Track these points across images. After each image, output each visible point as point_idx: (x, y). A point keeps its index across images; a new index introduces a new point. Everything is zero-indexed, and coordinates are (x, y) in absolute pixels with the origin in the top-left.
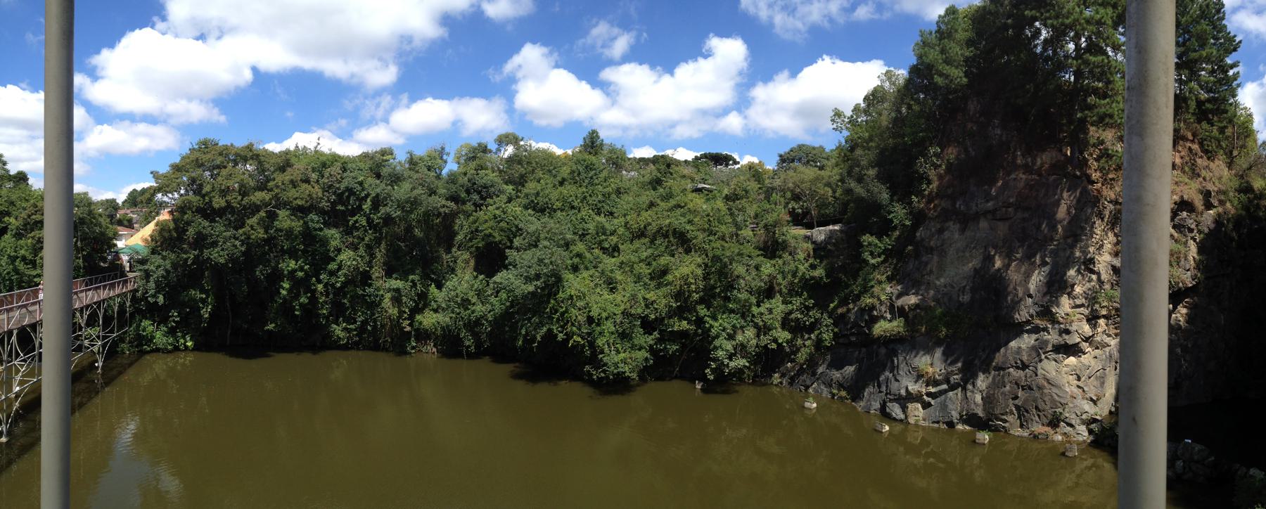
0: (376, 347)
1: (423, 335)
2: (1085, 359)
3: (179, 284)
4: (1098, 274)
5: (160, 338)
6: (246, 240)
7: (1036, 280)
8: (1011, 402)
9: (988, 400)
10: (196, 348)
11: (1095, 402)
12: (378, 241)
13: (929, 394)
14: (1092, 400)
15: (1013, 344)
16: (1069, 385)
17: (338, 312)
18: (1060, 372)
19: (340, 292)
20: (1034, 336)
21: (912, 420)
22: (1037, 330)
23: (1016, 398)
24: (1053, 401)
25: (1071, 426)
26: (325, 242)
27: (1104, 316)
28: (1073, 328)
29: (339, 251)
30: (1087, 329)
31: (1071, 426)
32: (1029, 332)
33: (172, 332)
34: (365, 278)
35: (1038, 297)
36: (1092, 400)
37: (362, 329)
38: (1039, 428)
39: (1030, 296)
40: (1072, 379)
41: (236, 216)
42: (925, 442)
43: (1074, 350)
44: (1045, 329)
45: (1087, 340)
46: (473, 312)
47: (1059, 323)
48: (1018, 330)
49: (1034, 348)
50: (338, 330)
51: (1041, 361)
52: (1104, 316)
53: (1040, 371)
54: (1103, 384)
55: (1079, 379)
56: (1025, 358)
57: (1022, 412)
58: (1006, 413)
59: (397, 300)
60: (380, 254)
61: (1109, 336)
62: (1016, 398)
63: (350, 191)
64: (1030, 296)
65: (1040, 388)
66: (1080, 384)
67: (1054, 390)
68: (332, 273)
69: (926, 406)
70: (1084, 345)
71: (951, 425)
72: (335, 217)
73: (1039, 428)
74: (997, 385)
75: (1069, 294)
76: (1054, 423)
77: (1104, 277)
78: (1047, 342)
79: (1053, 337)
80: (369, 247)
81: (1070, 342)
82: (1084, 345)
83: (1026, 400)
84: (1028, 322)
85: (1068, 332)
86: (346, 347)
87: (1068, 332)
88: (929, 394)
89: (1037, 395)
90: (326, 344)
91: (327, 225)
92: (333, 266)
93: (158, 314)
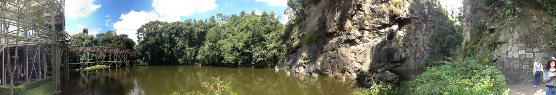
0: (188, 64)
1: (198, 61)
2: (358, 47)
3: (144, 51)
4: (364, 11)
5: (141, 63)
6: (156, 40)
7: (337, 15)
8: (329, 64)
9: (322, 64)
10: (149, 65)
11: (361, 64)
12: (186, 39)
13: (305, 63)
14: (360, 62)
15: (330, 42)
16: (351, 56)
17: (179, 56)
18: (347, 51)
19: (179, 51)
20: (337, 38)
21: (300, 72)
22: (338, 35)
23: (331, 62)
24: (343, 63)
25: (350, 73)
26: (175, 40)
27: (368, 30)
28: (352, 32)
29: (178, 42)
30: (359, 34)
31: (350, 73)
32: (335, 36)
33: (144, 61)
34: (184, 48)
35: (338, 22)
36: (360, 62)
37: (185, 60)
38: (338, 74)
39: (335, 21)
40: (352, 54)
41: (154, 34)
42: (305, 80)
43: (352, 42)
44: (341, 34)
45: (359, 38)
46: (177, 47)
47: (346, 31)
48: (331, 35)
49: (337, 42)
50: (180, 60)
51: (340, 47)
52: (368, 30)
53: (339, 51)
54: (365, 56)
55: (355, 55)
56: (334, 46)
57: (333, 67)
58: (327, 68)
59: (191, 53)
60: (187, 42)
61: (370, 38)
62: (331, 62)
63: (179, 28)
64: (335, 21)
65: (339, 58)
66: (356, 56)
67: (344, 58)
68: (177, 47)
69: (305, 67)
70: (358, 41)
71: (311, 73)
72: (177, 35)
73: (338, 74)
74: (325, 58)
75: (350, 19)
76: (343, 72)
77: (367, 13)
78: (341, 39)
79: (344, 37)
80: (184, 41)
81: (351, 39)
82: (358, 41)
83: (334, 63)
84: (335, 32)
85: (349, 34)
86: (182, 64)
87: (349, 34)
88: (305, 63)
89: (338, 61)
90: (178, 64)
91: (176, 36)
92: (177, 45)
93: (141, 57)
